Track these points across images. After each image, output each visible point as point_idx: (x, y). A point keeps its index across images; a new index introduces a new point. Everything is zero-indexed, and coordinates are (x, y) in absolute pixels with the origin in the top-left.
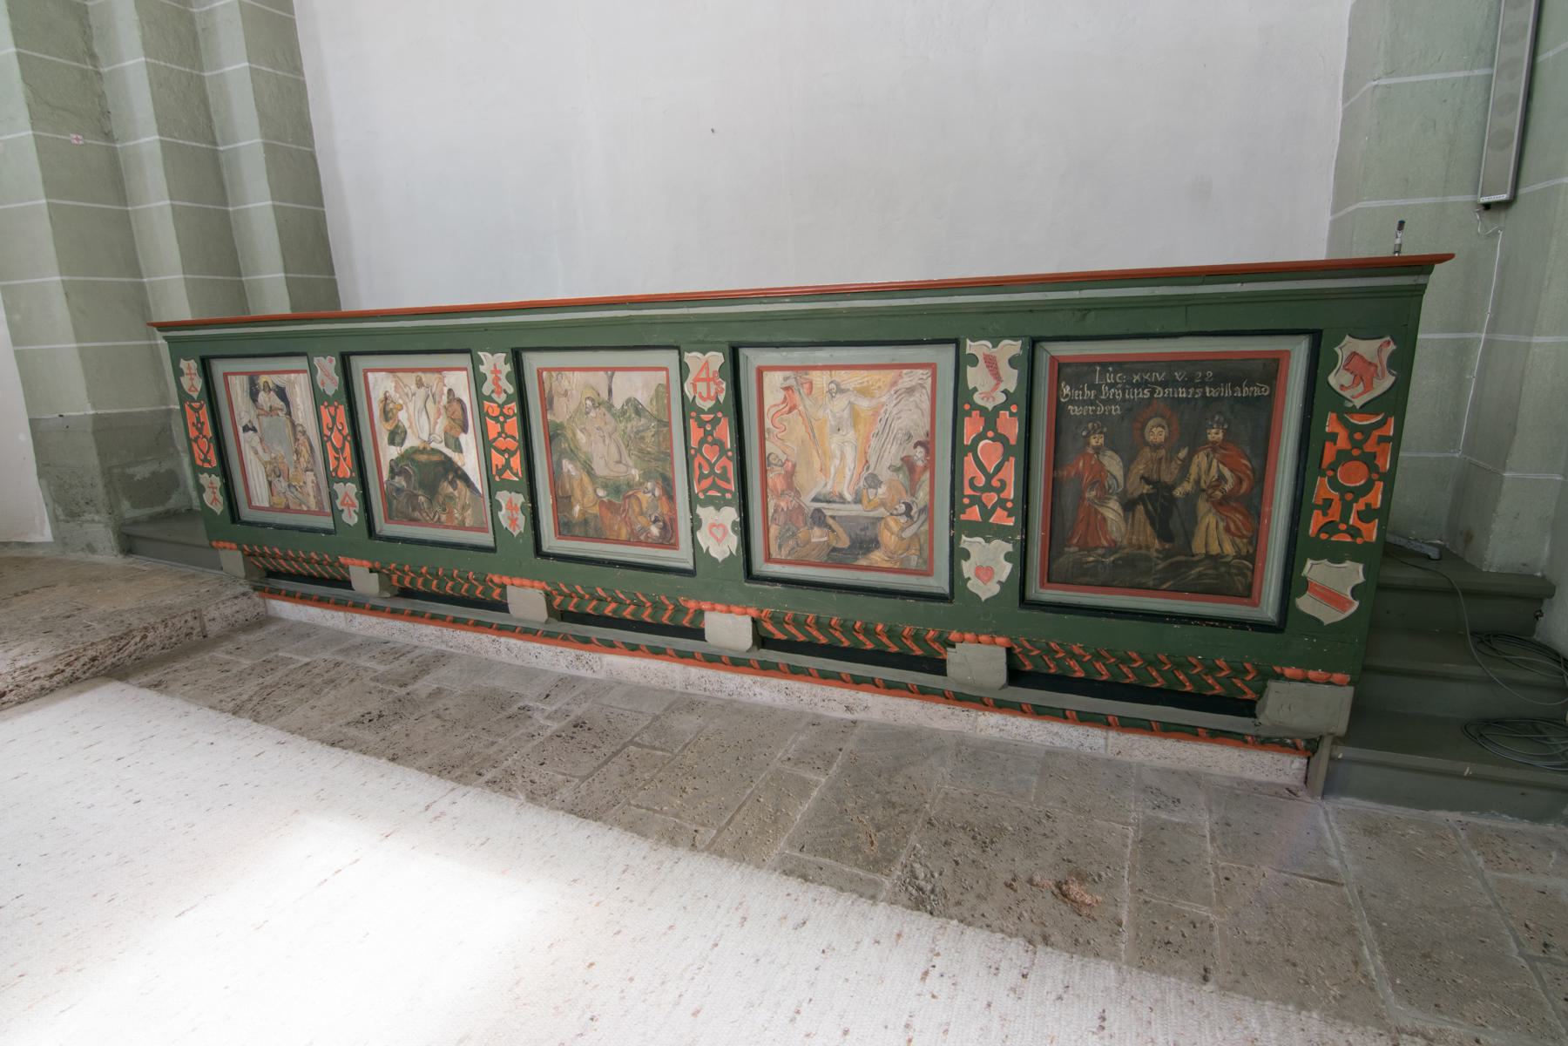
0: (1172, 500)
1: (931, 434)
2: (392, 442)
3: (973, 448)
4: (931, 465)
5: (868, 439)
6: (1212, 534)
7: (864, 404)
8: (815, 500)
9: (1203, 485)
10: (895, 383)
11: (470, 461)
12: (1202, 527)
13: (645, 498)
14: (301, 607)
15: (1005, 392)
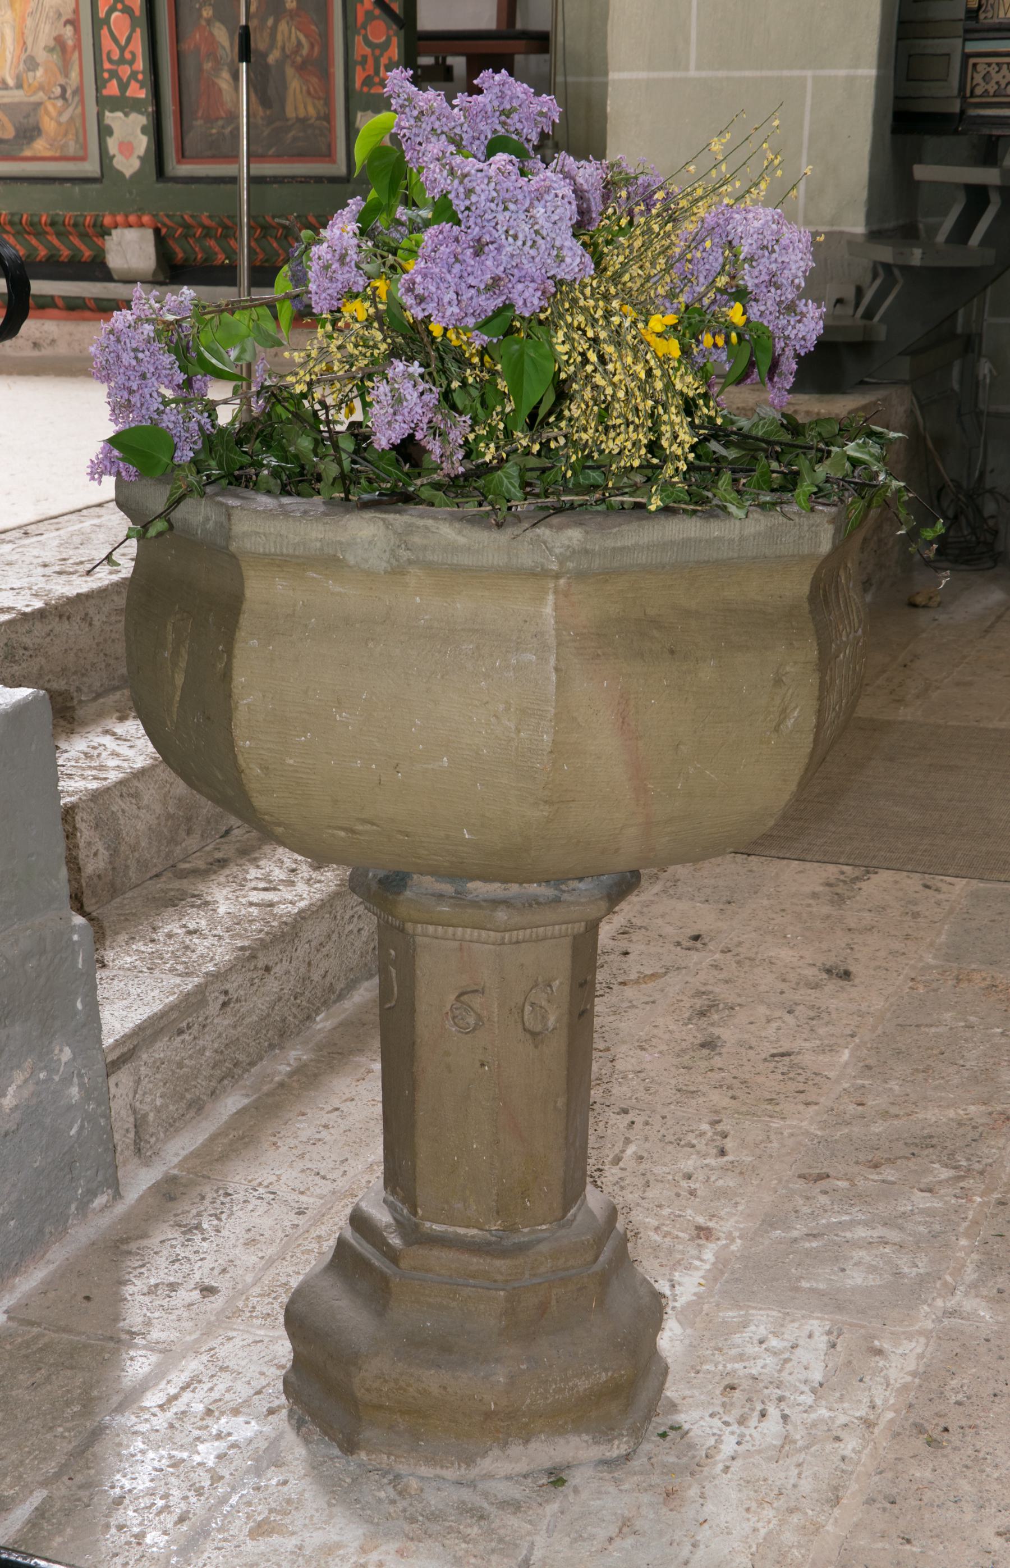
0: (267, 66)
1: (76, 11)
3: (107, 20)
4: (78, 45)
5: (24, 20)
9: (288, 52)
12: (291, 92)
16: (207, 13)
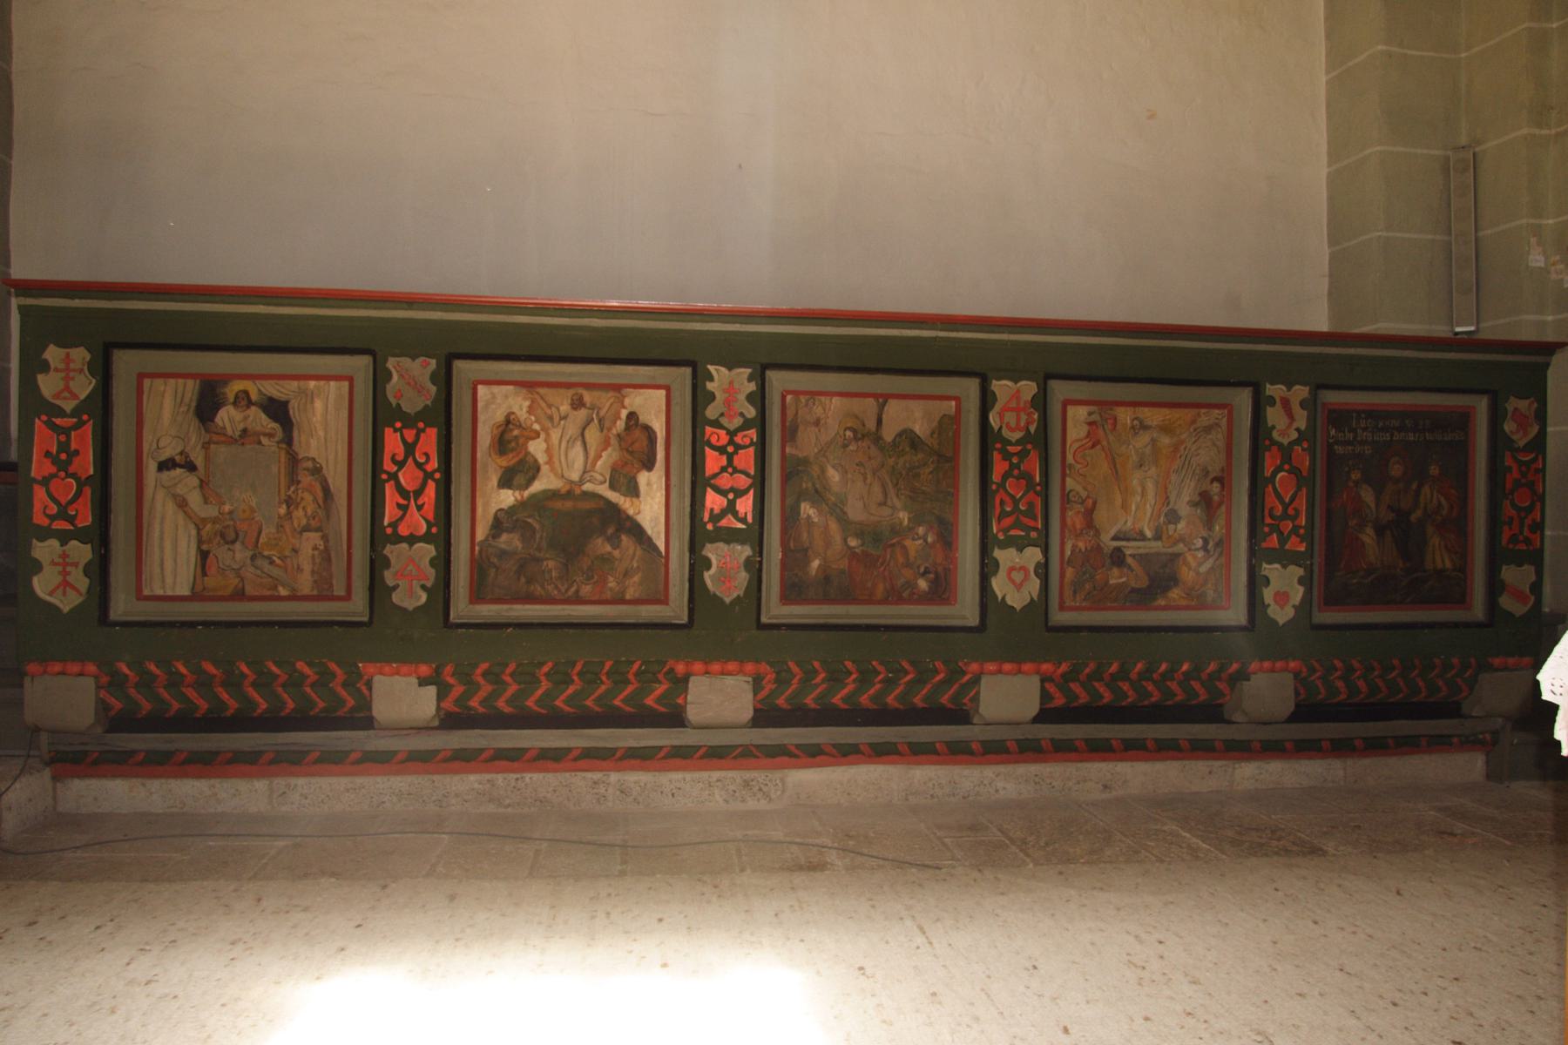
2: (506, 482)
6: (1438, 557)
7: (1166, 440)
8: (1115, 538)
10: (1194, 422)
11: (650, 507)
13: (913, 546)
14: (155, 785)
15: (1297, 430)
16: (1356, 476)
